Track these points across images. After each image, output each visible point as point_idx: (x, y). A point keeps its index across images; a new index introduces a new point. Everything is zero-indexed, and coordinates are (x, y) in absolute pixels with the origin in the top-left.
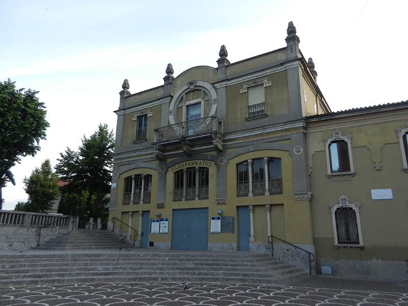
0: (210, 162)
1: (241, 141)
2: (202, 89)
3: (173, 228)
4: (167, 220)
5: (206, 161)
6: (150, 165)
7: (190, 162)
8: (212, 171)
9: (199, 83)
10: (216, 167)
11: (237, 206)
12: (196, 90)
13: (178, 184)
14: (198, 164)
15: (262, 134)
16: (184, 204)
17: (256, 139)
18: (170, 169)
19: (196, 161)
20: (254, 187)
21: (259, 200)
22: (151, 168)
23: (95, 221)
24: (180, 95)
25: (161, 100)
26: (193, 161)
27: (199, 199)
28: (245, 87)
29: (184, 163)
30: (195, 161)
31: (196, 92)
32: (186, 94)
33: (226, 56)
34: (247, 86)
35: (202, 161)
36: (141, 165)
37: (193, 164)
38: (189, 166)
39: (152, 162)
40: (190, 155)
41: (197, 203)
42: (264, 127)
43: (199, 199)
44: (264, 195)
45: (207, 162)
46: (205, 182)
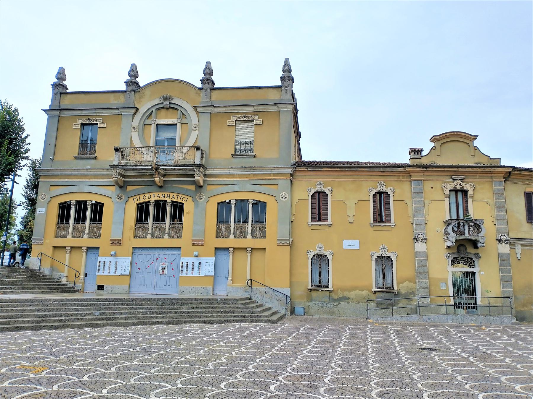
0: (187, 197)
5: (180, 195)
6: (102, 190)
7: (161, 194)
9: (175, 101)
15: (250, 174)
19: (169, 194)
21: (77, 242)
29: (151, 194)
30: (166, 194)
31: (170, 110)
35: (175, 195)
37: (163, 196)
45: (183, 196)
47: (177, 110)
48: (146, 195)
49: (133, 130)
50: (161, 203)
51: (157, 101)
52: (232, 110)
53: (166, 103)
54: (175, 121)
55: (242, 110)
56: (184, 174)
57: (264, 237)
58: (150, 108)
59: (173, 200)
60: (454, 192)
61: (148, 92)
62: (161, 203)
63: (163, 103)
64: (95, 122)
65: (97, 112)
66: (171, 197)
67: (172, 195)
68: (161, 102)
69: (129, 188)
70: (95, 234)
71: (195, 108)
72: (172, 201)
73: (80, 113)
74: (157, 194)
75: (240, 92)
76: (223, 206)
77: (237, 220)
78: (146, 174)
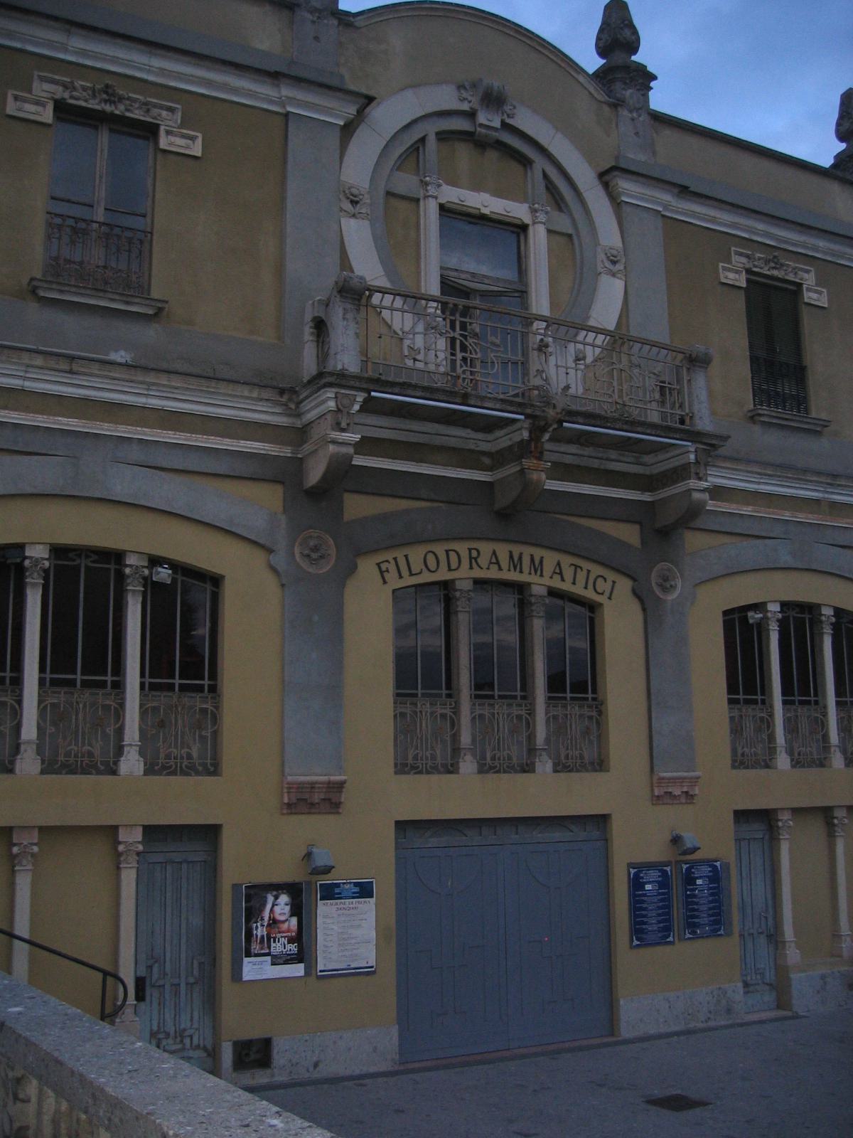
0: (611, 576)
1: (747, 510)
2: (540, 163)
3: (404, 936)
4: (364, 891)
5: (586, 565)
6: (219, 502)
7: (503, 550)
8: (621, 626)
9: (526, 121)
10: (635, 606)
11: (397, 823)
12: (500, 146)
13: (420, 676)
14: (548, 572)
15: (818, 501)
16: (466, 793)
17: (801, 517)
18: (367, 567)
19: (538, 553)
20: (154, 722)
21: (80, 799)
22: (232, 537)
23: (659, 876)
24: (407, 127)
25: (286, 91)
26: (516, 550)
27: (560, 767)
28: (42, 89)
29: (462, 547)
30: (527, 551)
31: (492, 155)
32: (443, 136)
33: (633, 47)
34: (60, 92)
35: (566, 560)
36: (124, 483)
37: (516, 564)
38: (493, 574)
39: (228, 486)
40: (512, 514)
41: (544, 792)
42: (835, 476)
43: (560, 767)
44: (114, 772)
45: (597, 570)
46: (577, 682)
47: (525, 162)
48: (440, 549)
49: (347, 206)
50: (83, 563)
51: (446, 98)
52: (734, 226)
53: (489, 119)
54: (519, 211)
55: (767, 235)
56: (595, 464)
57: (213, 769)
58: (415, 122)
59: (557, 583)
60: (573, 567)
61: (397, 39)
62: (736, 616)
63: (471, 115)
64: (137, 114)
65: (157, 63)
66: (549, 567)
67: (550, 559)
68: (465, 107)
69: (357, 506)
70: (191, 749)
71: (605, 178)
72: (553, 593)
73: (50, 44)
74: (486, 548)
75: (748, 160)
76: (741, 629)
77: (58, 658)
78: (438, 441)
